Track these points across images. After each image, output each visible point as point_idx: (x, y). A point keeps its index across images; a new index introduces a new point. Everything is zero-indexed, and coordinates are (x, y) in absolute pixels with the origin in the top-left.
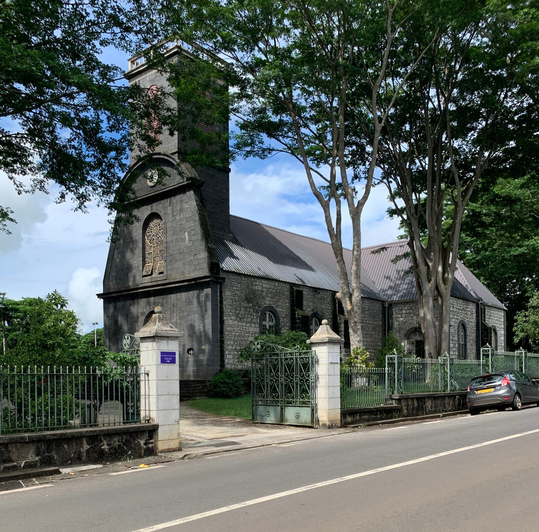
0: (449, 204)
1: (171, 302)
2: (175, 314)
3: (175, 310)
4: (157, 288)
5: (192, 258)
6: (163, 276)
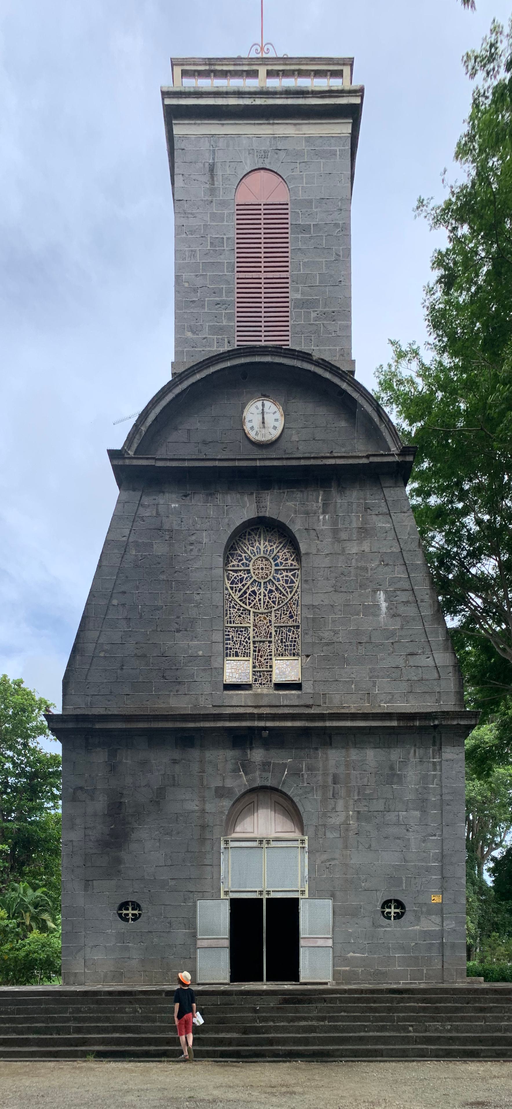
2: (340, 803)
3: (343, 792)
5: (400, 662)
6: (299, 696)
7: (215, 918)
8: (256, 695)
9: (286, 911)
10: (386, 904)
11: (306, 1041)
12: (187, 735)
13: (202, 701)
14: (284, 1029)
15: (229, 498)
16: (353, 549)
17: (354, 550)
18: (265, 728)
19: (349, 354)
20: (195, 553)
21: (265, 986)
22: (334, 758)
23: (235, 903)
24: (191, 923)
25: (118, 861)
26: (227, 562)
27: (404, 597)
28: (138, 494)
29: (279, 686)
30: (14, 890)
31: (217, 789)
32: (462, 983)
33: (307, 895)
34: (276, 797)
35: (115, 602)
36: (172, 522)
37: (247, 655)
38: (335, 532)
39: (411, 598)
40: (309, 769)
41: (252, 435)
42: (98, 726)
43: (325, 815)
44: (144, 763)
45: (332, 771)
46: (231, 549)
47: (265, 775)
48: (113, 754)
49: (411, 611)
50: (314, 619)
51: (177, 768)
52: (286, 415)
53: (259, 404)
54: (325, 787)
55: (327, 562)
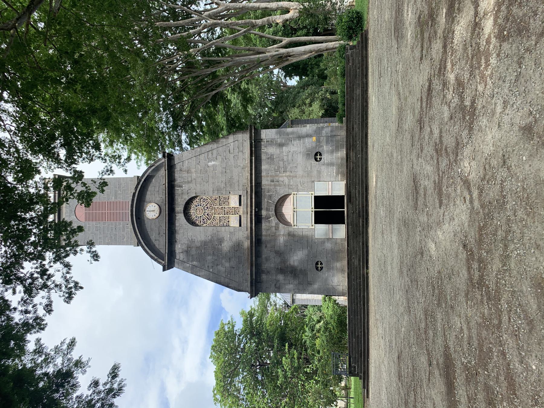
0: (169, 137)
1: (269, 185)
3: (277, 178)
4: (254, 218)
5: (232, 156)
7: (322, 229)
8: (243, 213)
9: (320, 201)
10: (316, 160)
11: (363, 194)
12: (257, 240)
14: (359, 202)
15: (177, 225)
18: (255, 210)
19: (132, 178)
21: (345, 210)
22: (265, 182)
23: (316, 222)
24: (323, 242)
25: (301, 270)
26: (197, 225)
29: (240, 205)
30: (305, 342)
32: (344, 124)
33: (313, 193)
34: (278, 205)
35: (211, 270)
37: (229, 218)
38: (188, 182)
39: (211, 152)
40: (269, 192)
41: (157, 215)
43: (285, 185)
45: (269, 183)
46: (193, 223)
47: (271, 210)
49: (215, 152)
50: (218, 190)
52: (150, 202)
53: (147, 212)
54: (275, 185)
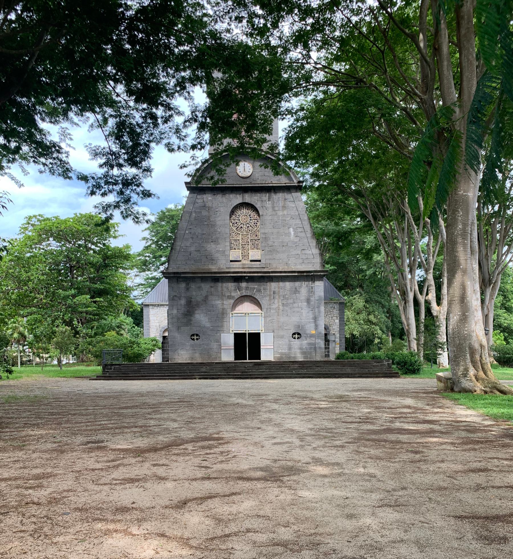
3: (277, 297)
5: (299, 252)
8: (243, 264)
9: (255, 337)
12: (217, 278)
13: (222, 266)
16: (280, 213)
17: (281, 214)
20: (218, 215)
21: (248, 361)
22: (273, 286)
23: (236, 335)
24: (218, 341)
25: (191, 320)
26: (230, 217)
27: (300, 230)
28: (196, 195)
29: (251, 261)
31: (228, 296)
34: (251, 298)
35: (187, 232)
36: (209, 204)
38: (273, 207)
41: (240, 174)
42: (182, 275)
43: (270, 305)
44: (200, 288)
45: (273, 290)
46: (232, 212)
48: (188, 284)
49: (303, 234)
51: (212, 289)
52: (253, 167)
54: (270, 295)
55: (270, 218)
